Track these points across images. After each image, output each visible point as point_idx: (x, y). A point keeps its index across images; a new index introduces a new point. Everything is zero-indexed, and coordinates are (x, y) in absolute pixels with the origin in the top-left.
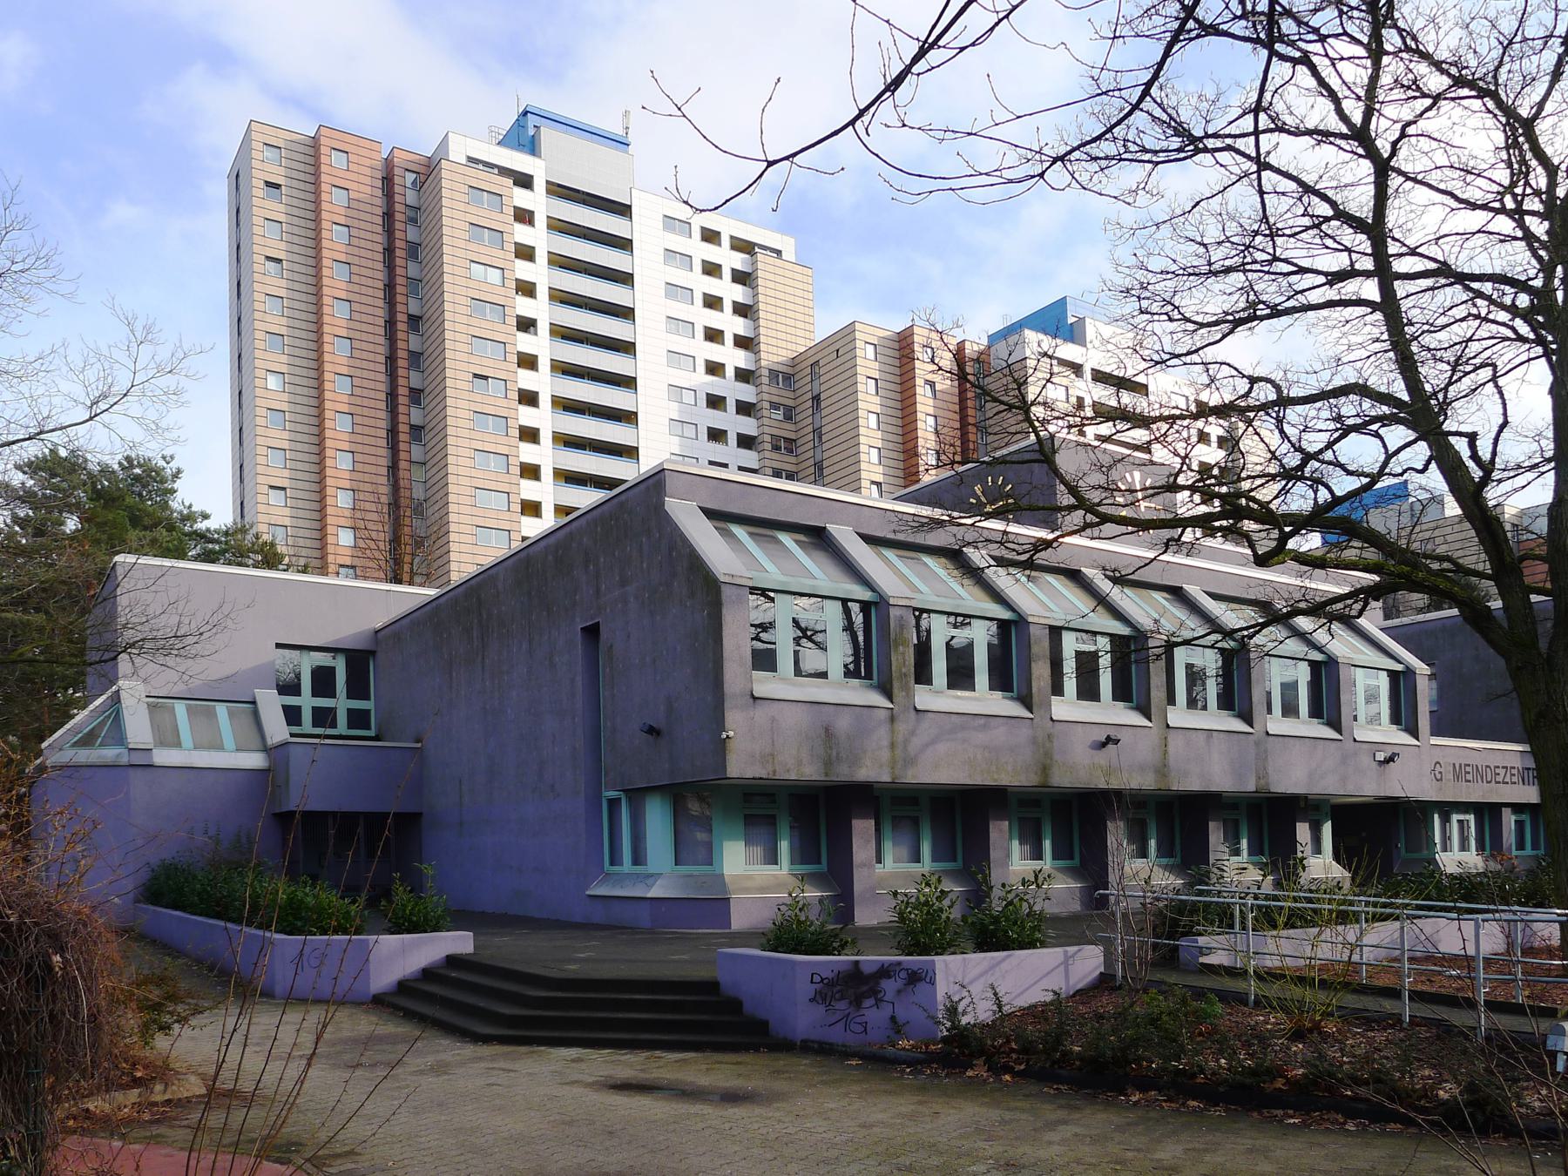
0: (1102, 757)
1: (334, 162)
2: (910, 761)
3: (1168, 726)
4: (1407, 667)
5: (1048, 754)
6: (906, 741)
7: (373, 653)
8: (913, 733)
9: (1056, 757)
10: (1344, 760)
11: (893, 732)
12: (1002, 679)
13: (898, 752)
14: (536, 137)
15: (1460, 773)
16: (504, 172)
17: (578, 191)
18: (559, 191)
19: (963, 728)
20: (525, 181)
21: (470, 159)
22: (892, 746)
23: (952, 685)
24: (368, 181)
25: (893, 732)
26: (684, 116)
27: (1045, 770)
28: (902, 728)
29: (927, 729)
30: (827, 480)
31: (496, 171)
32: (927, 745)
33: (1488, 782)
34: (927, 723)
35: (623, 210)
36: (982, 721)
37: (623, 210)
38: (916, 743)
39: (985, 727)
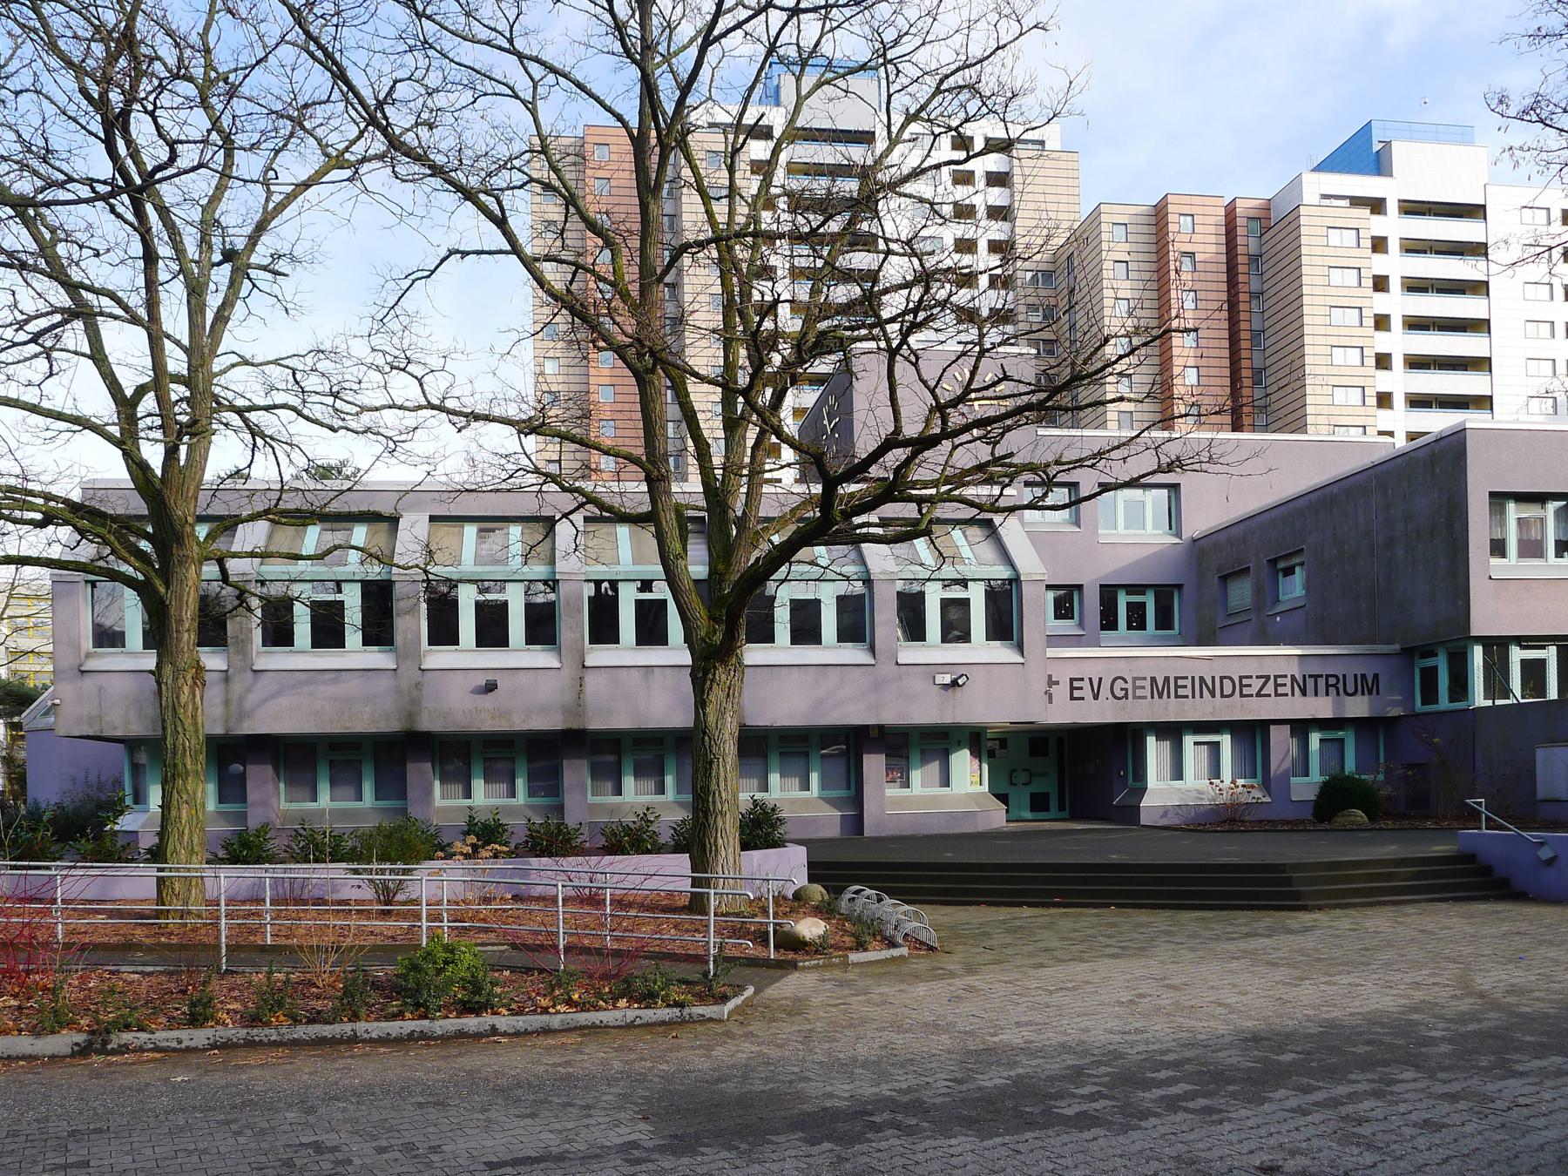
0: (487, 701)
1: (1179, 226)
2: (243, 716)
3: (584, 666)
4: (642, 581)
5: (416, 702)
6: (241, 699)
7: (1179, 587)
8: (249, 690)
9: (425, 703)
10: (878, 686)
11: (227, 690)
12: (378, 631)
13: (233, 708)
14: (1383, 157)
15: (1162, 688)
16: (1356, 202)
17: (1423, 202)
18: (1413, 208)
19: (307, 683)
20: (1377, 206)
21: (1325, 197)
22: (227, 702)
23: (316, 643)
24: (1213, 239)
25: (227, 690)
26: (1021, 34)
27: (411, 716)
28: (237, 687)
29: (265, 685)
30: (1083, 423)
31: (1346, 203)
32: (265, 701)
33: (1223, 696)
34: (264, 680)
35: (1474, 211)
36: (332, 675)
37: (1474, 211)
38: (251, 700)
39: (335, 681)
